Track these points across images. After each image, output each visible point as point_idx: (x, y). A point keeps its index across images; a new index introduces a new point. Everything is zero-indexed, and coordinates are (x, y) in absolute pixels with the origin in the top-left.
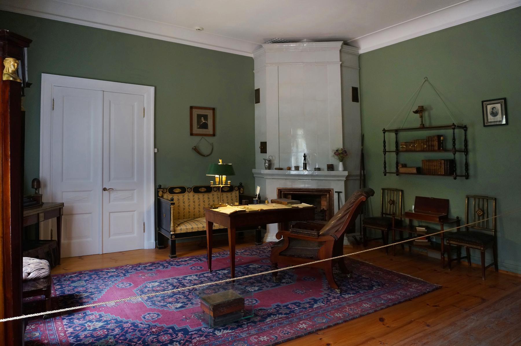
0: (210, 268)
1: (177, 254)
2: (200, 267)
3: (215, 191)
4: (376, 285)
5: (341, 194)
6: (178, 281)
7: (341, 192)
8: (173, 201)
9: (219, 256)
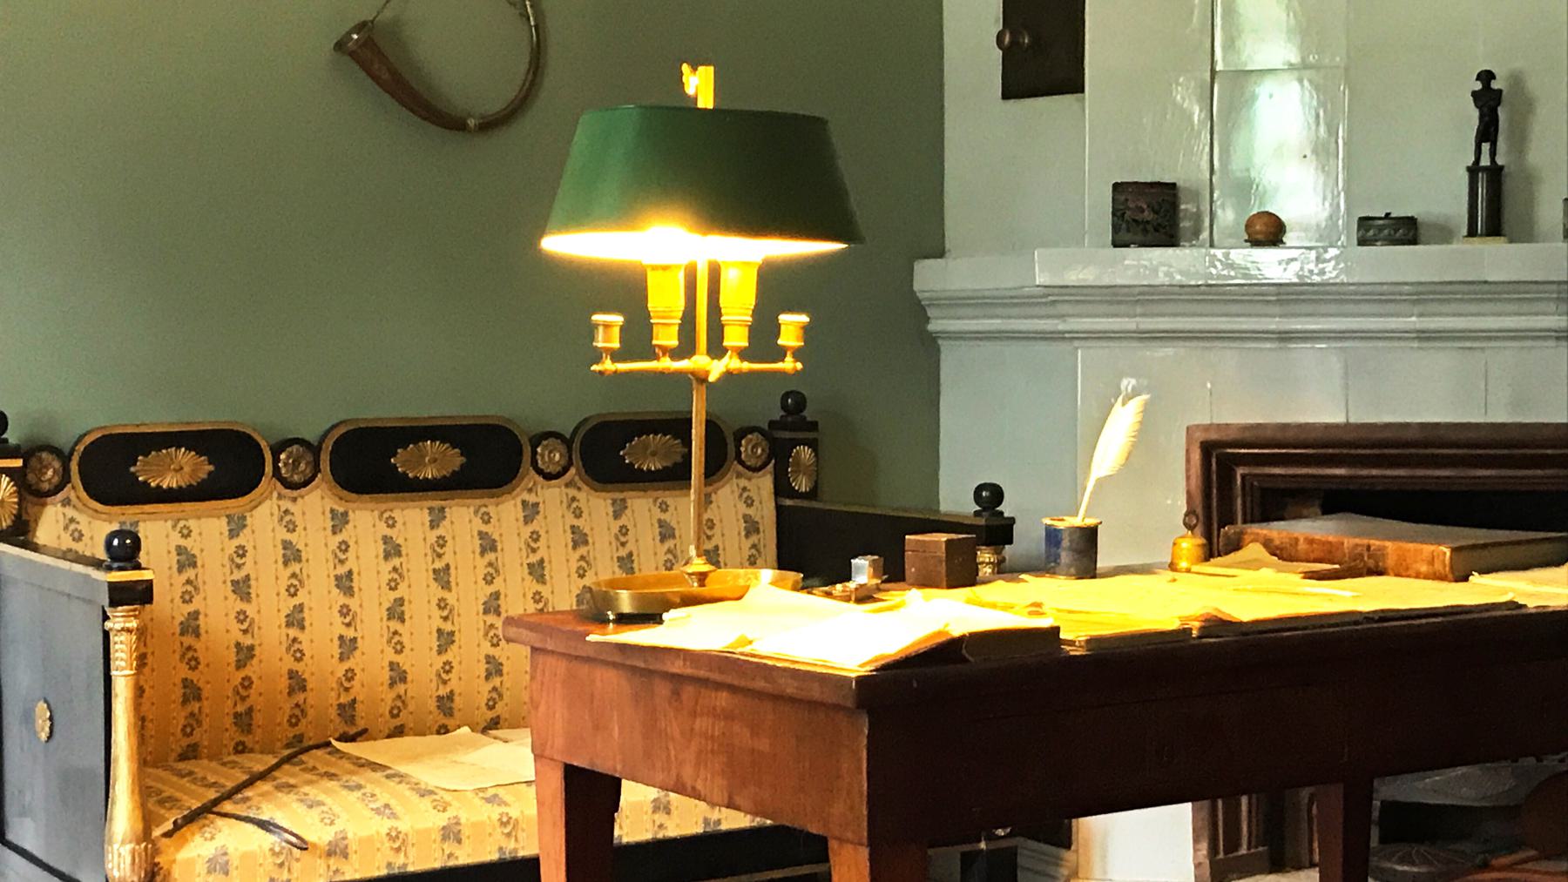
3: (549, 477)
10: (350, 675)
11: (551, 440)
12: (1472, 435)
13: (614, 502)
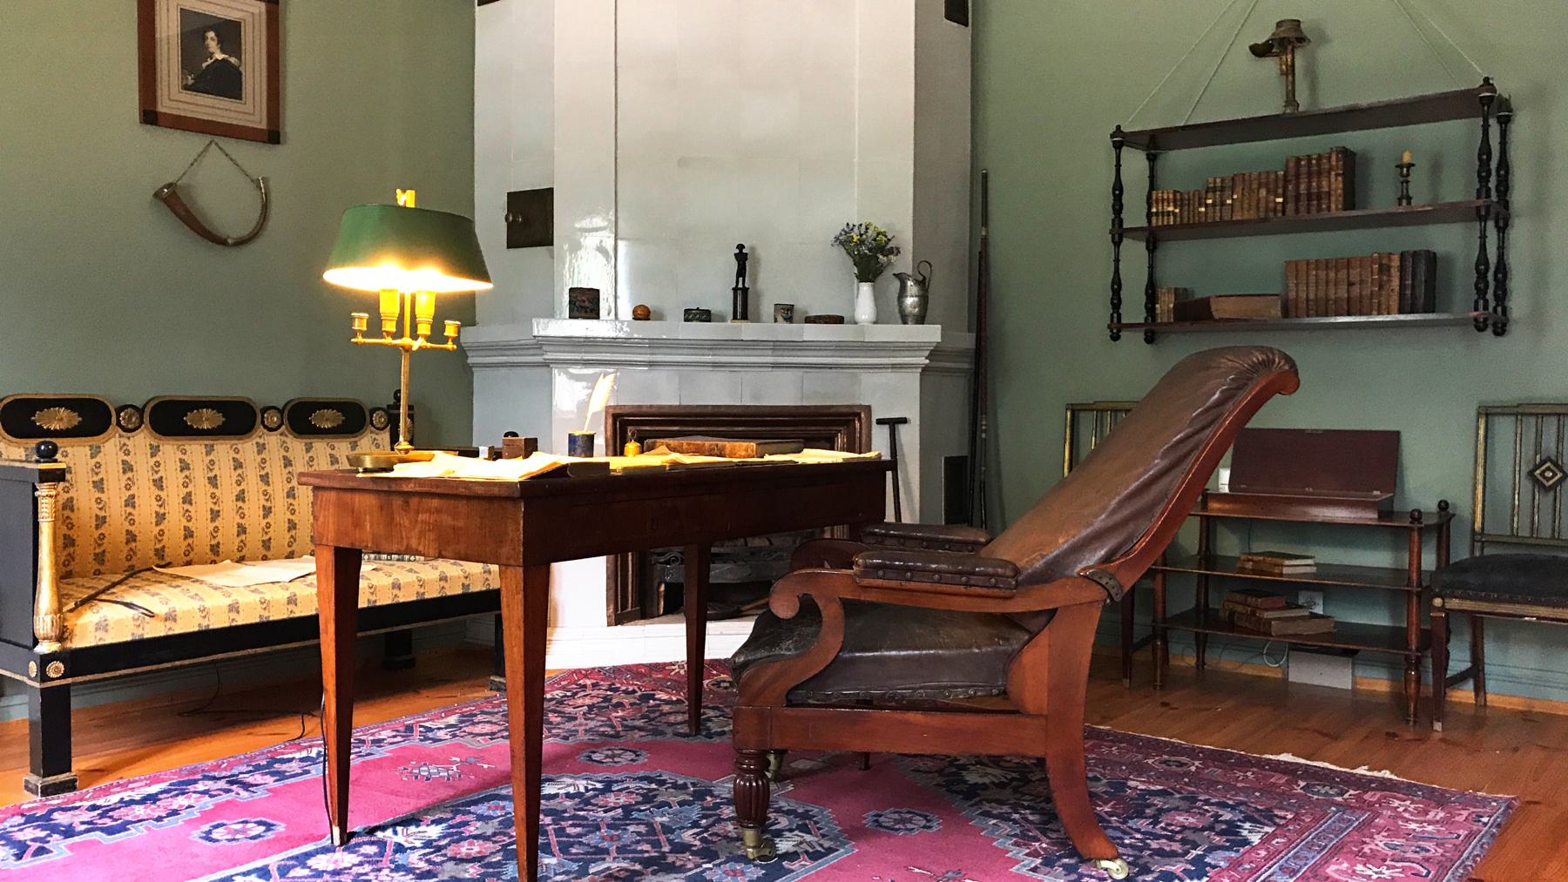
1: (79, 765)
2: (260, 823)
3: (271, 430)
7: (904, 421)
11: (272, 411)
12: (735, 411)
13: (306, 444)
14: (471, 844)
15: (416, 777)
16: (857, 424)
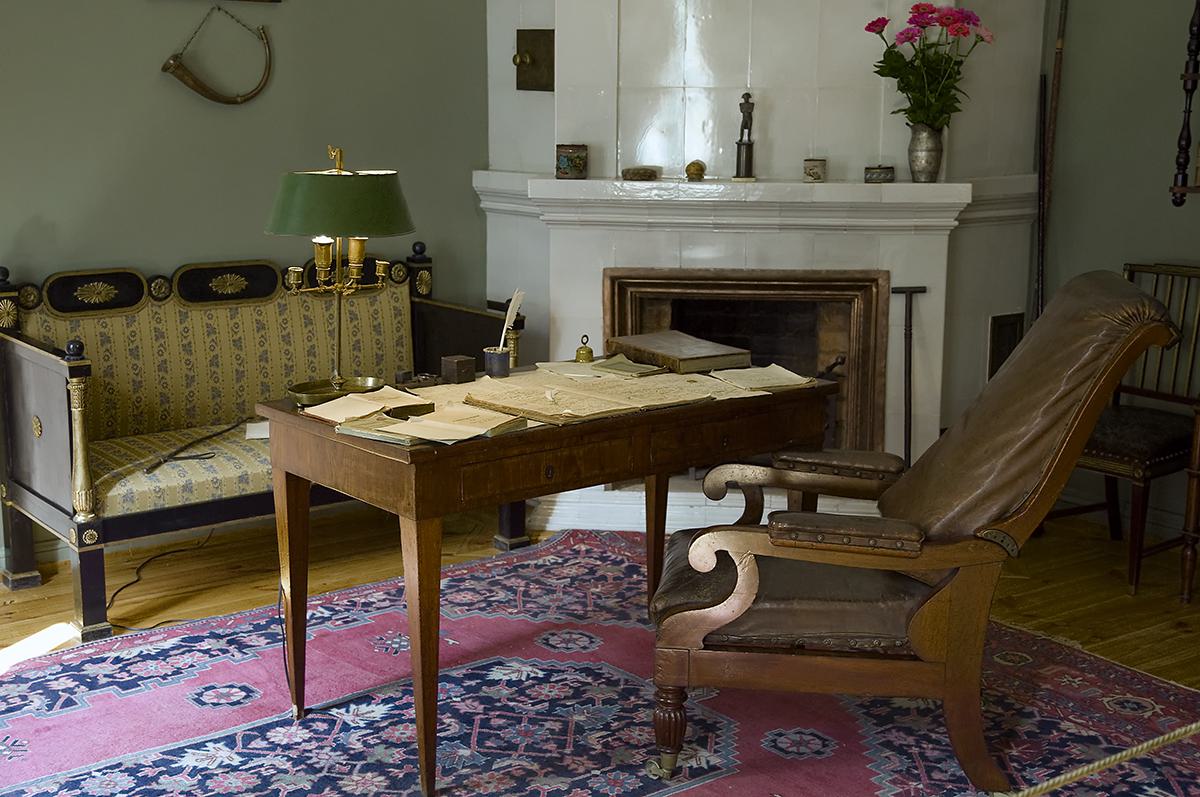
0: (299, 698)
4: (1150, 785)
5: (919, 299)
6: (138, 785)
7: (923, 290)
8: (83, 358)
9: (329, 619)
10: (242, 389)
14: (406, 728)
15: (387, 649)
16: (874, 290)
